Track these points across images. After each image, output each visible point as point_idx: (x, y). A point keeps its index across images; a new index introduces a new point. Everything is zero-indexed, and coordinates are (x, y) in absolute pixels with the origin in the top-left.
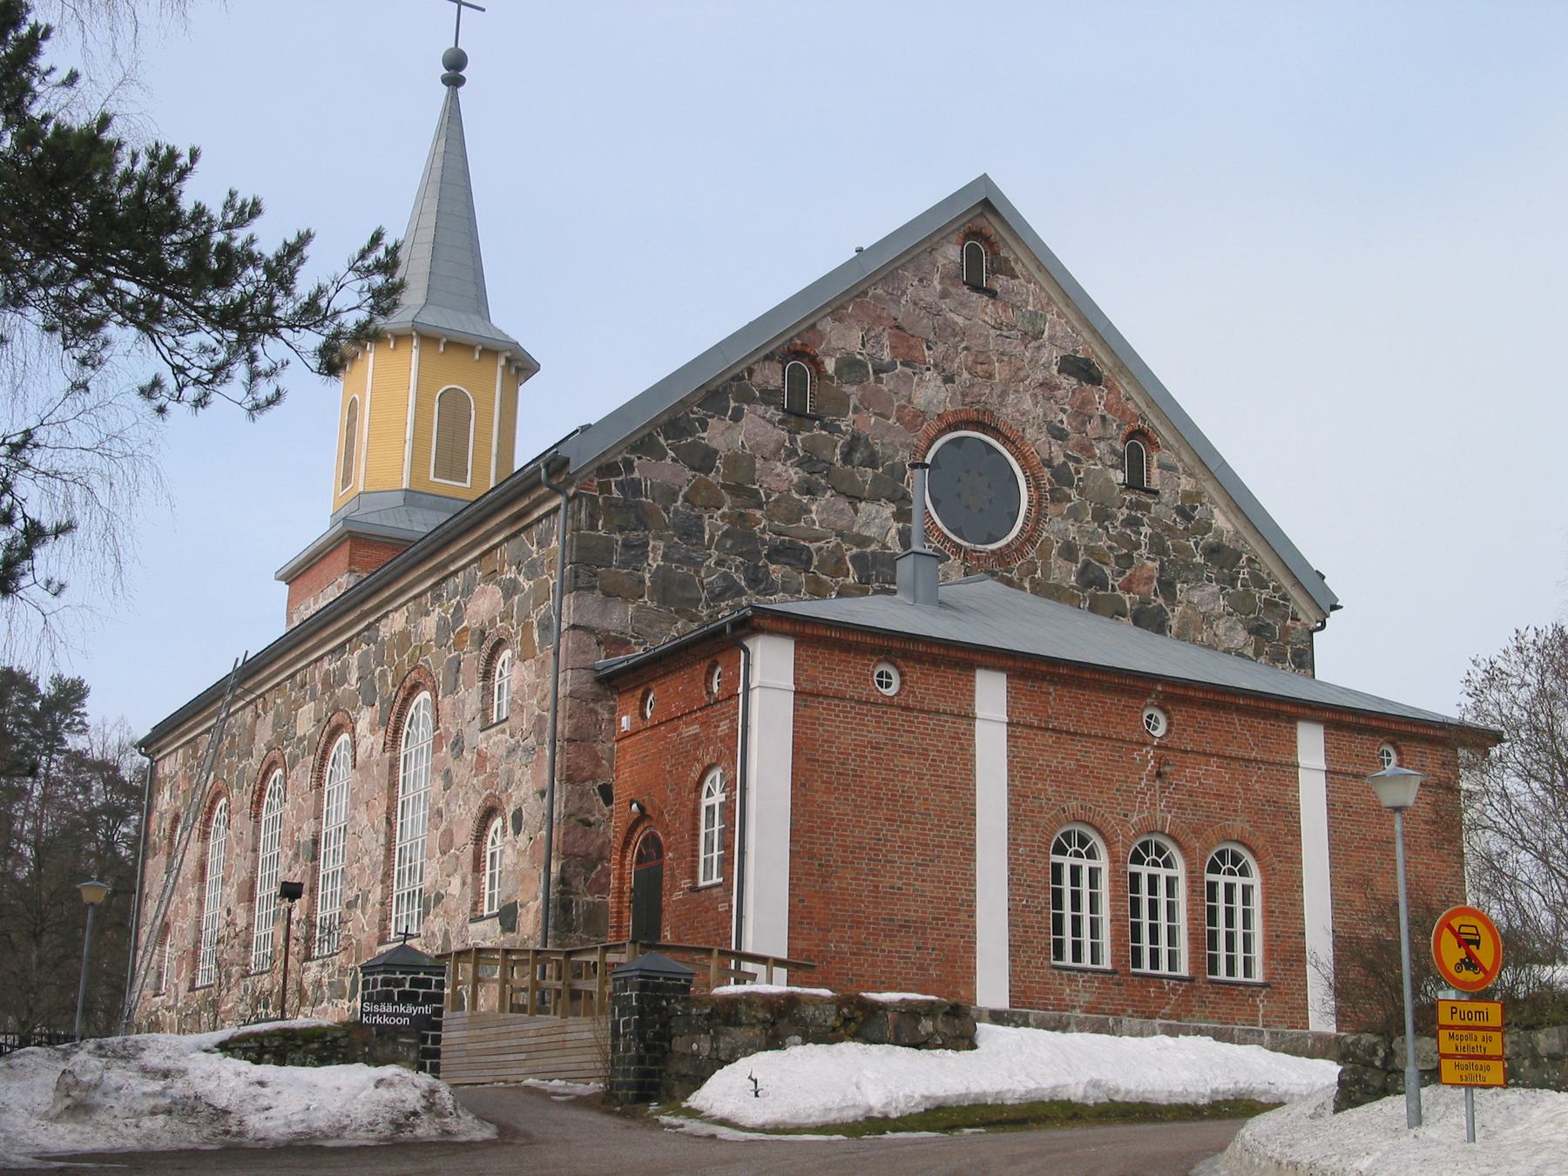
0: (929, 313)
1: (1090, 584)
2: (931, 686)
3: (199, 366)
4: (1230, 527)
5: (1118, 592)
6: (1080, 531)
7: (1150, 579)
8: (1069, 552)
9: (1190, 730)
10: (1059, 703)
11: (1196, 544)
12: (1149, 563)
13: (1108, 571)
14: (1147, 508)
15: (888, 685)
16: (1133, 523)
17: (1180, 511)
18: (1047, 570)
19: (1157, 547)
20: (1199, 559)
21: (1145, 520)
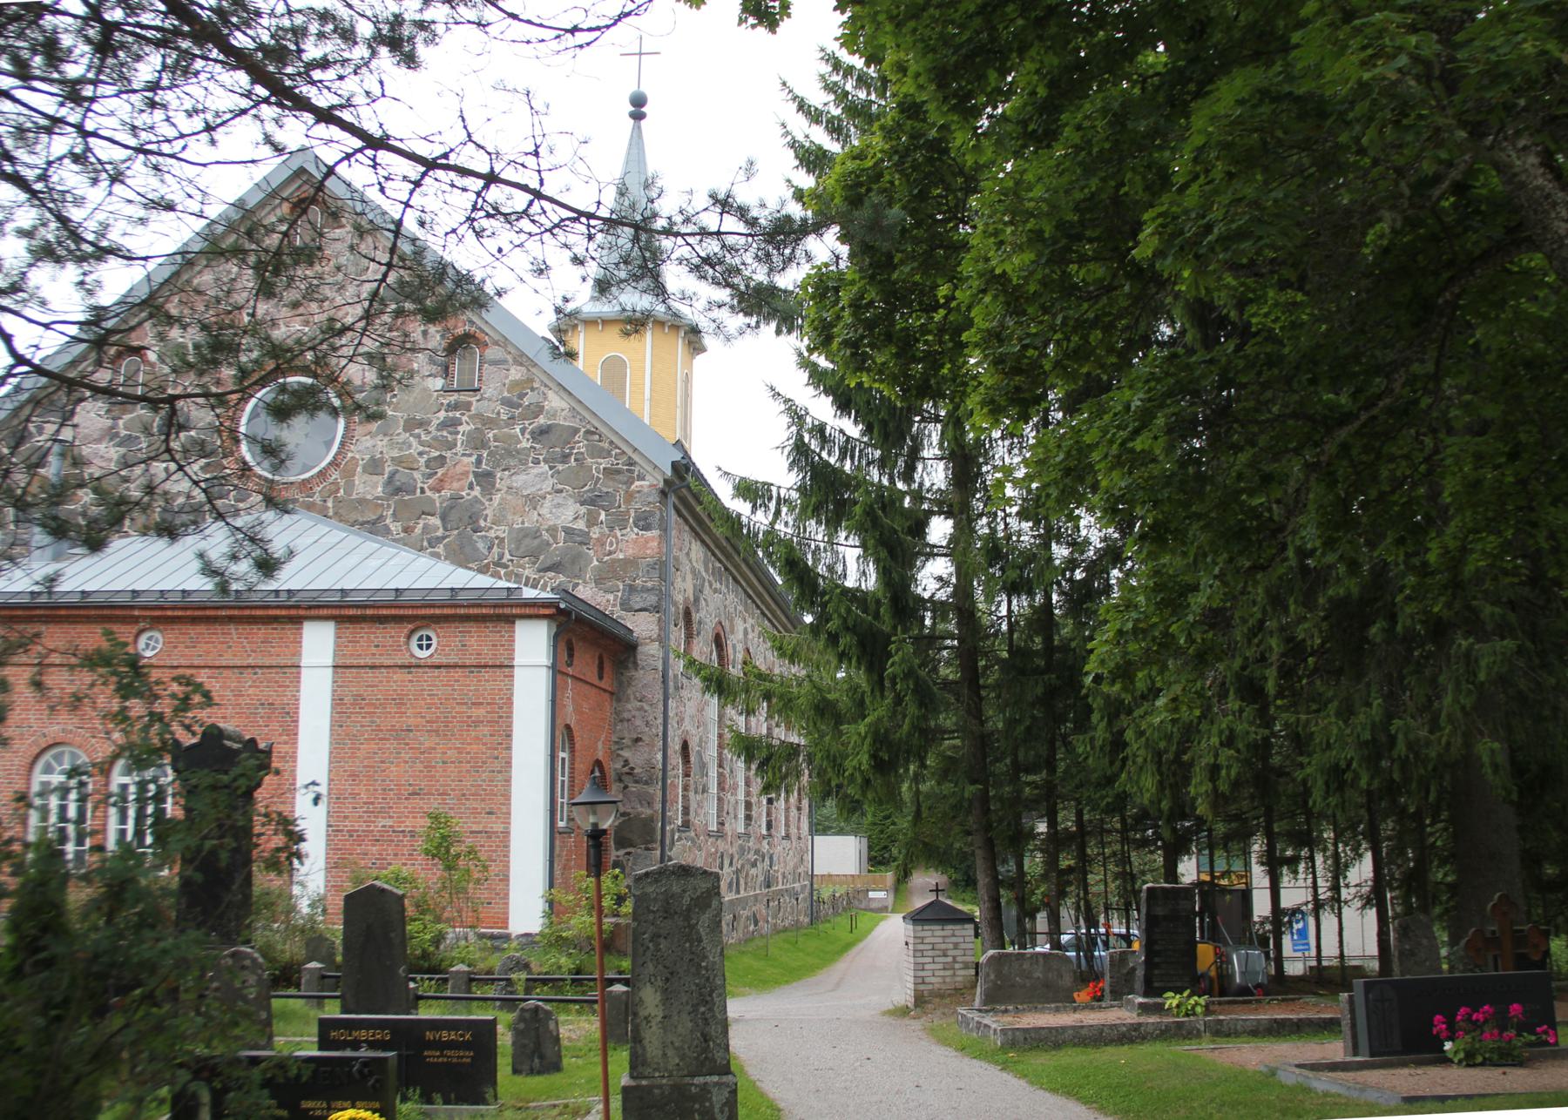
0: (232, 327)
1: (398, 490)
2: (477, 642)
3: (753, 324)
4: (564, 405)
5: (428, 493)
6: (392, 444)
7: (466, 473)
8: (374, 466)
9: (181, 647)
10: (377, 642)
11: (523, 431)
12: (466, 460)
13: (417, 475)
14: (467, 406)
15: (421, 647)
16: (451, 424)
17: (507, 402)
18: (350, 485)
19: (477, 442)
20: (525, 444)
21: (465, 418)
